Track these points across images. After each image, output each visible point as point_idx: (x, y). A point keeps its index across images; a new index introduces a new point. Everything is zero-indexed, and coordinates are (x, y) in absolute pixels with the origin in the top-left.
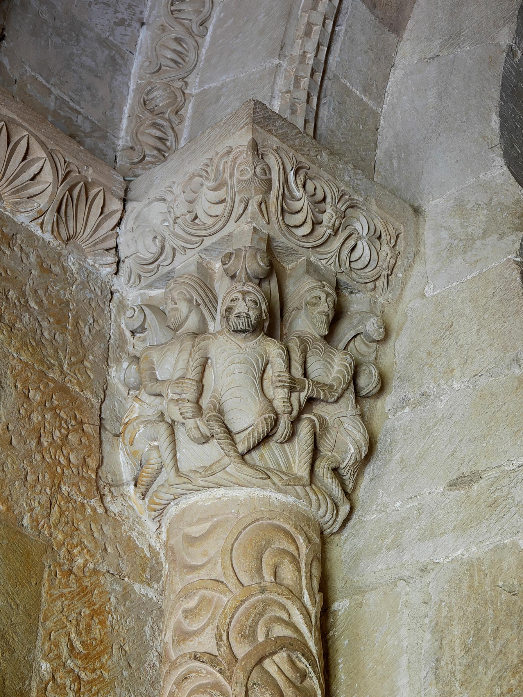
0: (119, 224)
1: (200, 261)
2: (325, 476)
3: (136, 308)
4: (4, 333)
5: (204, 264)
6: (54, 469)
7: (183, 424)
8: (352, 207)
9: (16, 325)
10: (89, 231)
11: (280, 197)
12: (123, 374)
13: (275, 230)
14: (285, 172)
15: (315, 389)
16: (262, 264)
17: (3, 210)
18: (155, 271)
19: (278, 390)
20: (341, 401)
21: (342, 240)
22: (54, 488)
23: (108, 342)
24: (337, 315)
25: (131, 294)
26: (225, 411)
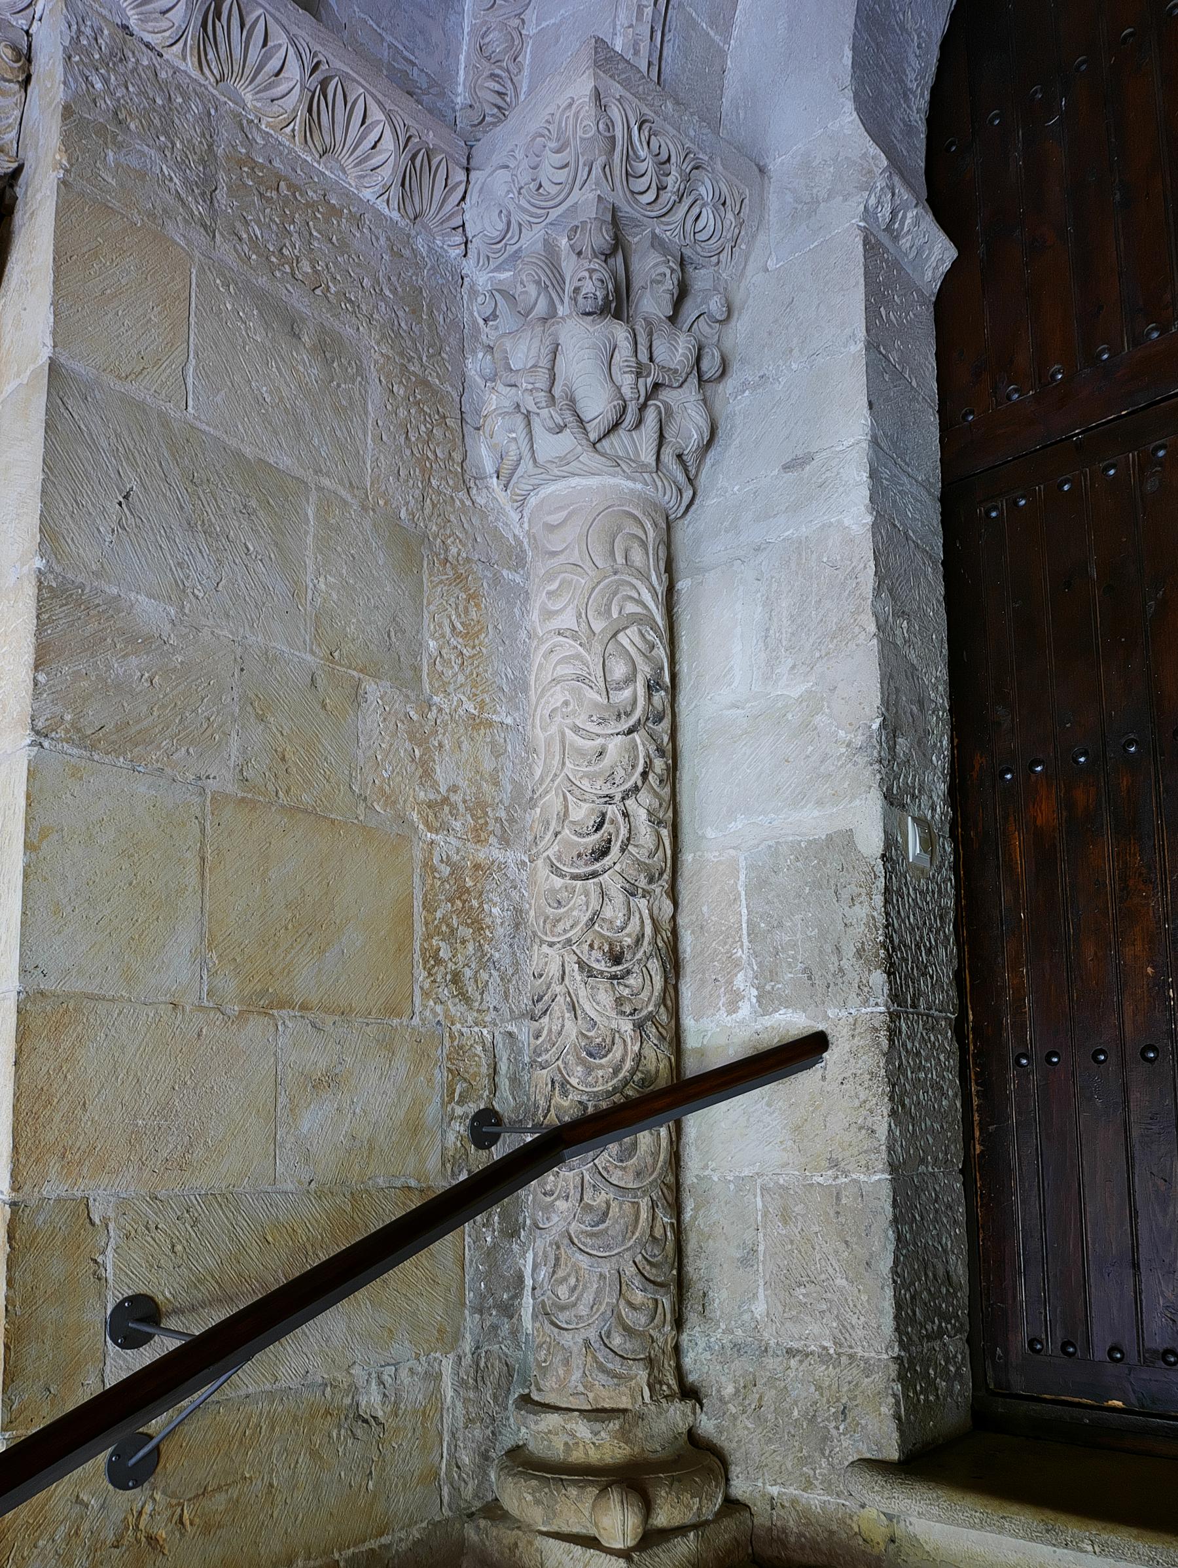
7: (538, 414)
8: (697, 168)
21: (686, 208)
25: (481, 278)
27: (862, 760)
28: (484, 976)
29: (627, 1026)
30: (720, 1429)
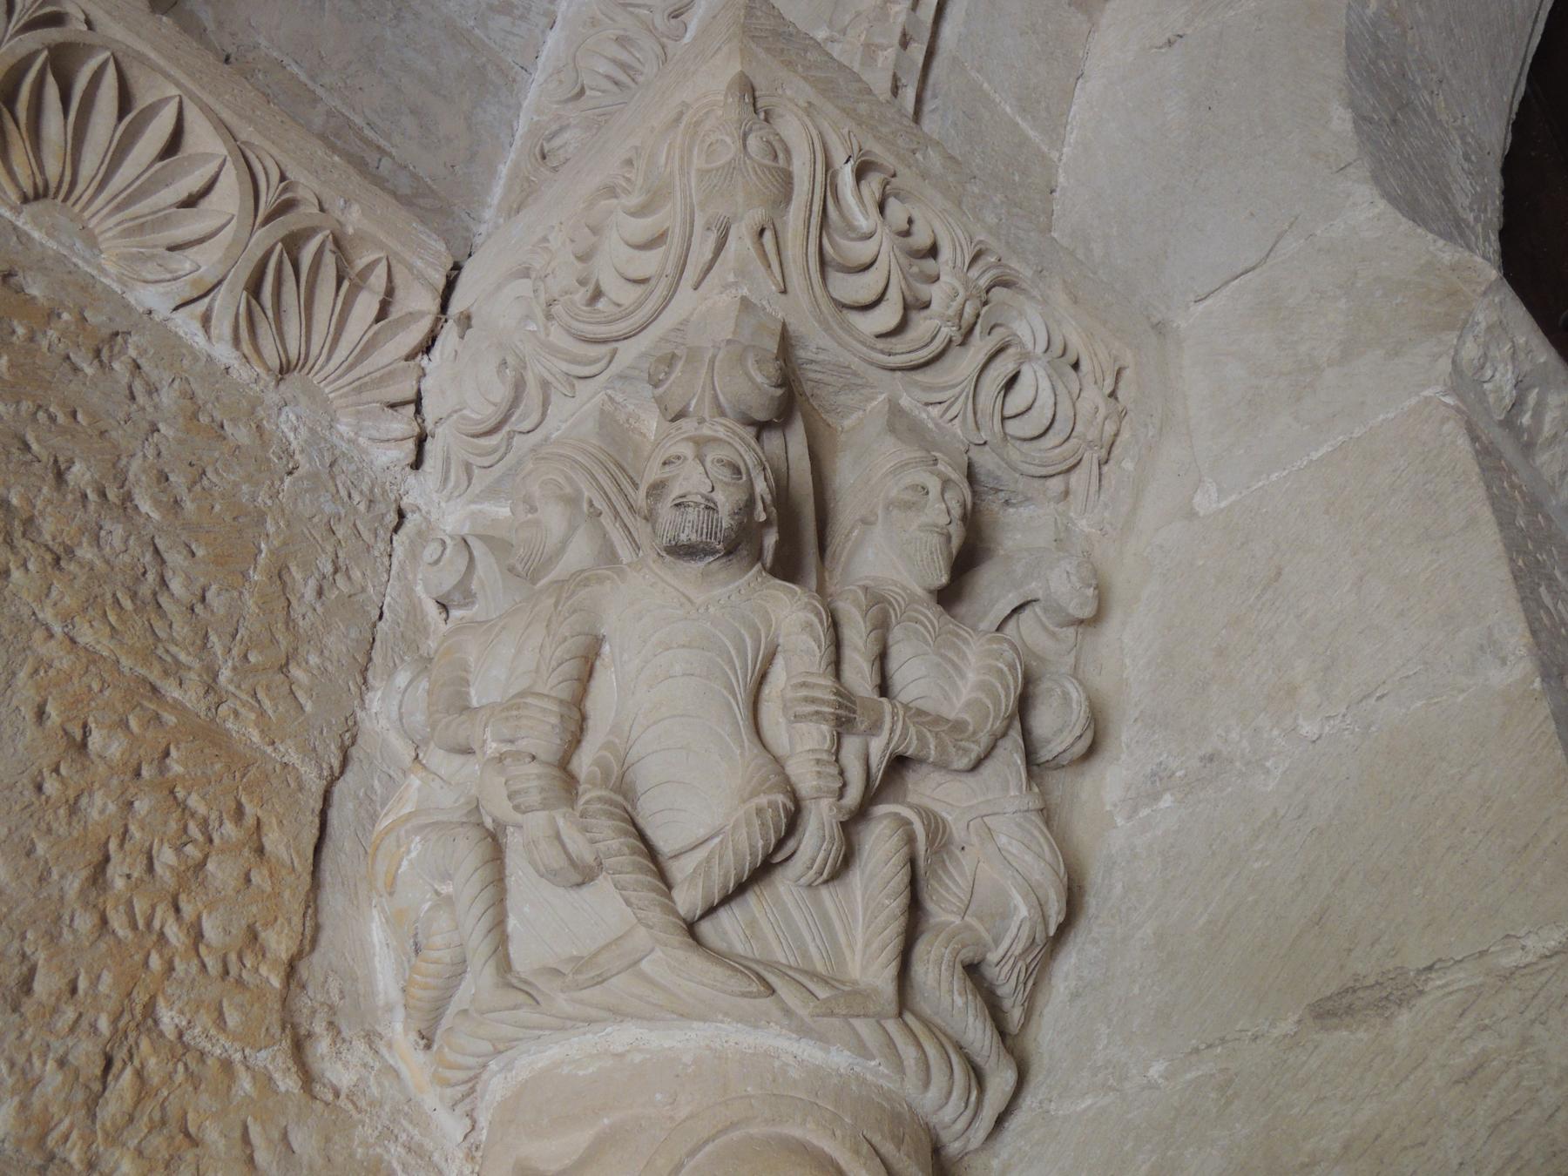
0: (427, 346)
1: (609, 407)
2: (945, 986)
3: (448, 541)
4: (30, 566)
5: (622, 418)
6: (137, 958)
7: (519, 826)
8: (1006, 284)
9: (79, 552)
10: (345, 353)
11: (816, 220)
12: (396, 703)
13: (800, 311)
14: (828, 165)
15: (912, 730)
16: (759, 379)
17: (94, 273)
18: (503, 450)
19: (802, 726)
20: (988, 769)
21: (981, 358)
22: (127, 1017)
23: (374, 626)
24: (968, 557)
25: (443, 507)
26: (640, 789)
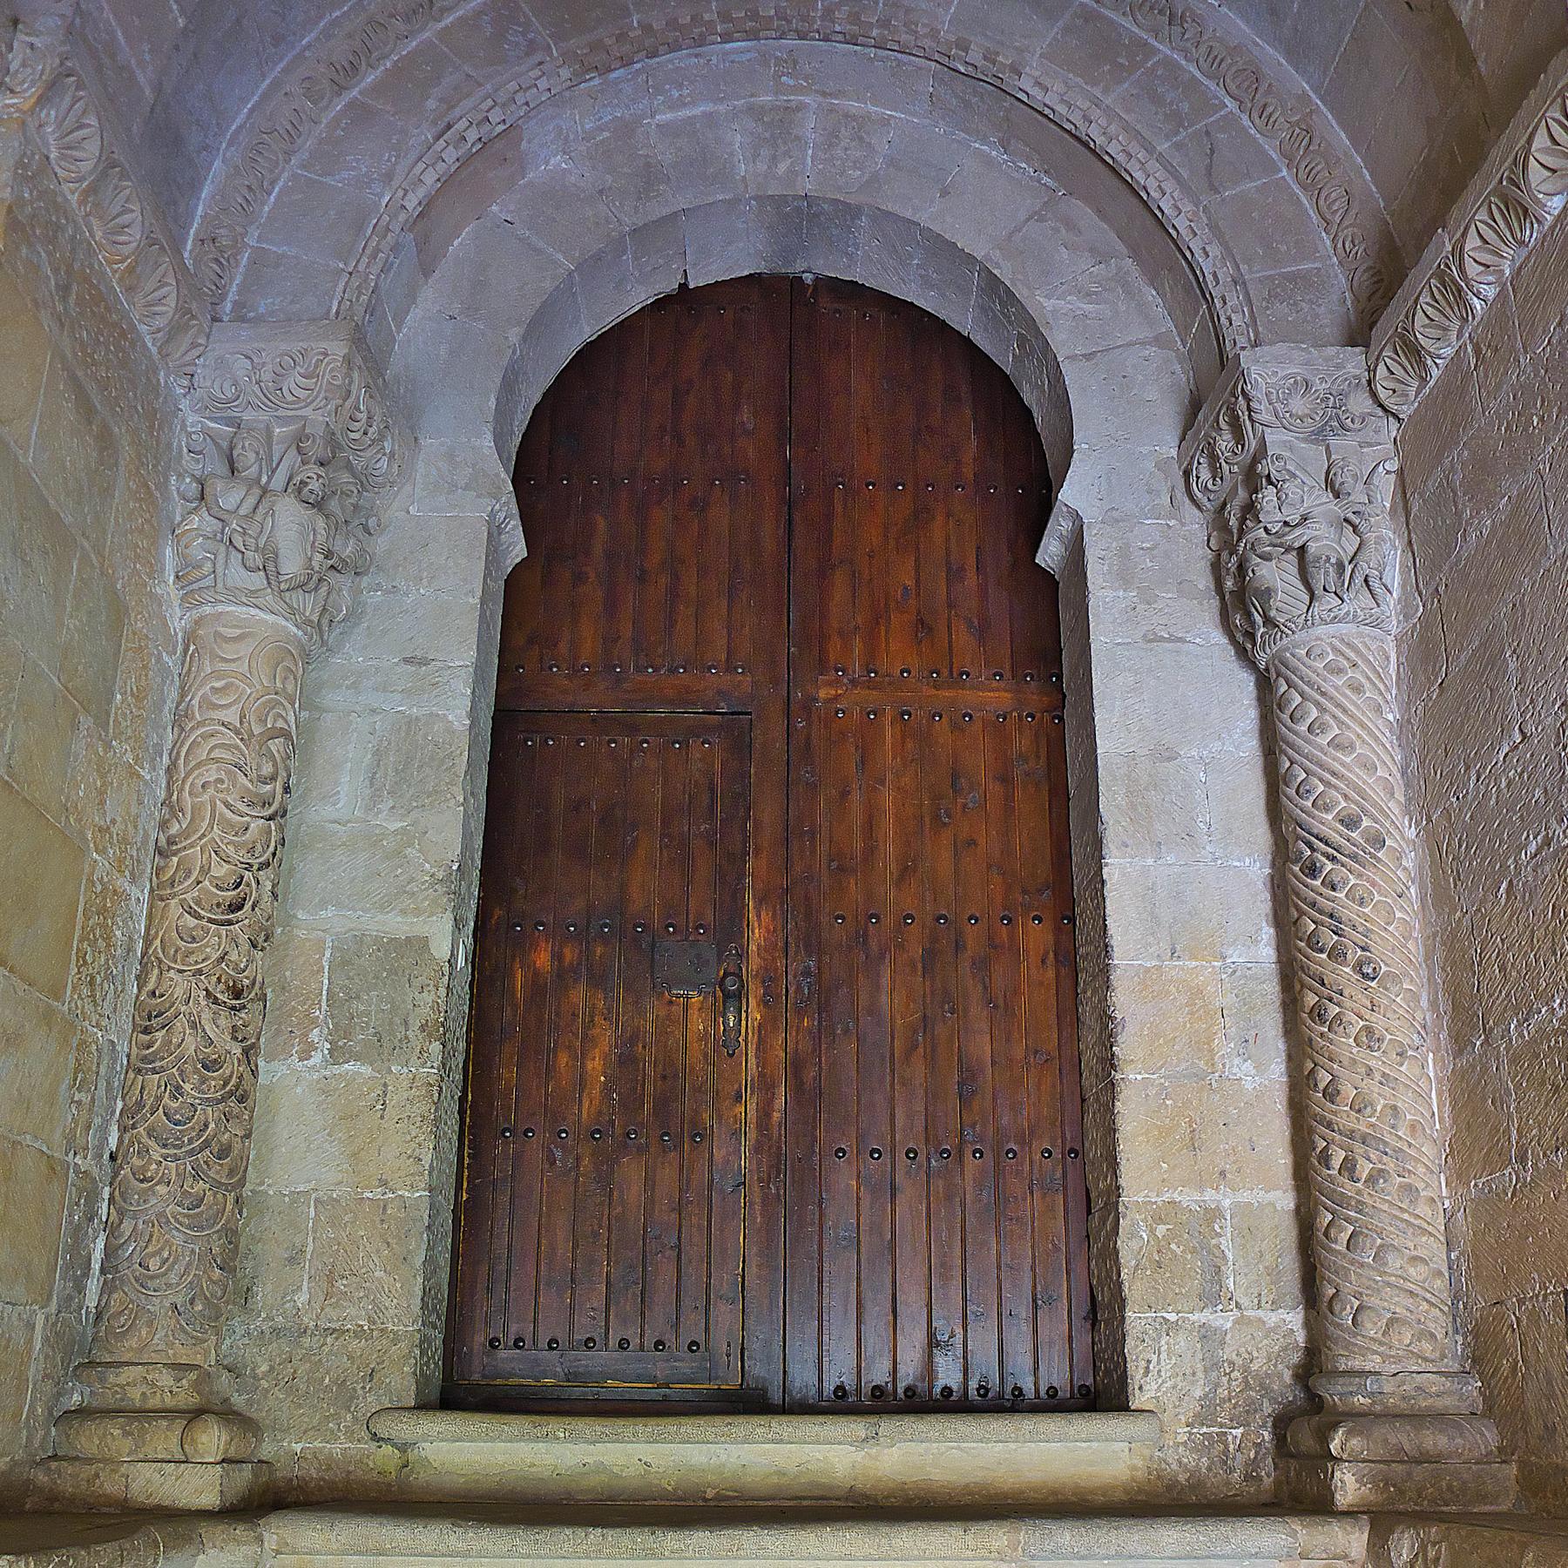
27: (441, 889)
28: (106, 986)
29: (237, 1050)
30: (250, 1403)
